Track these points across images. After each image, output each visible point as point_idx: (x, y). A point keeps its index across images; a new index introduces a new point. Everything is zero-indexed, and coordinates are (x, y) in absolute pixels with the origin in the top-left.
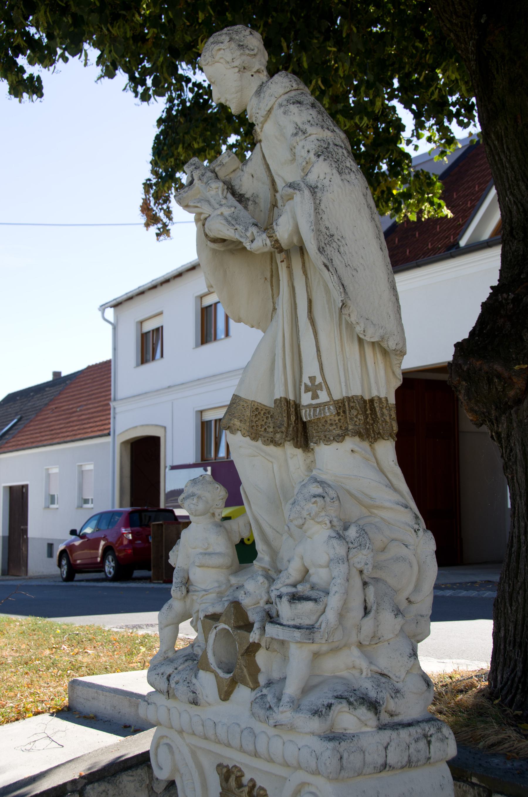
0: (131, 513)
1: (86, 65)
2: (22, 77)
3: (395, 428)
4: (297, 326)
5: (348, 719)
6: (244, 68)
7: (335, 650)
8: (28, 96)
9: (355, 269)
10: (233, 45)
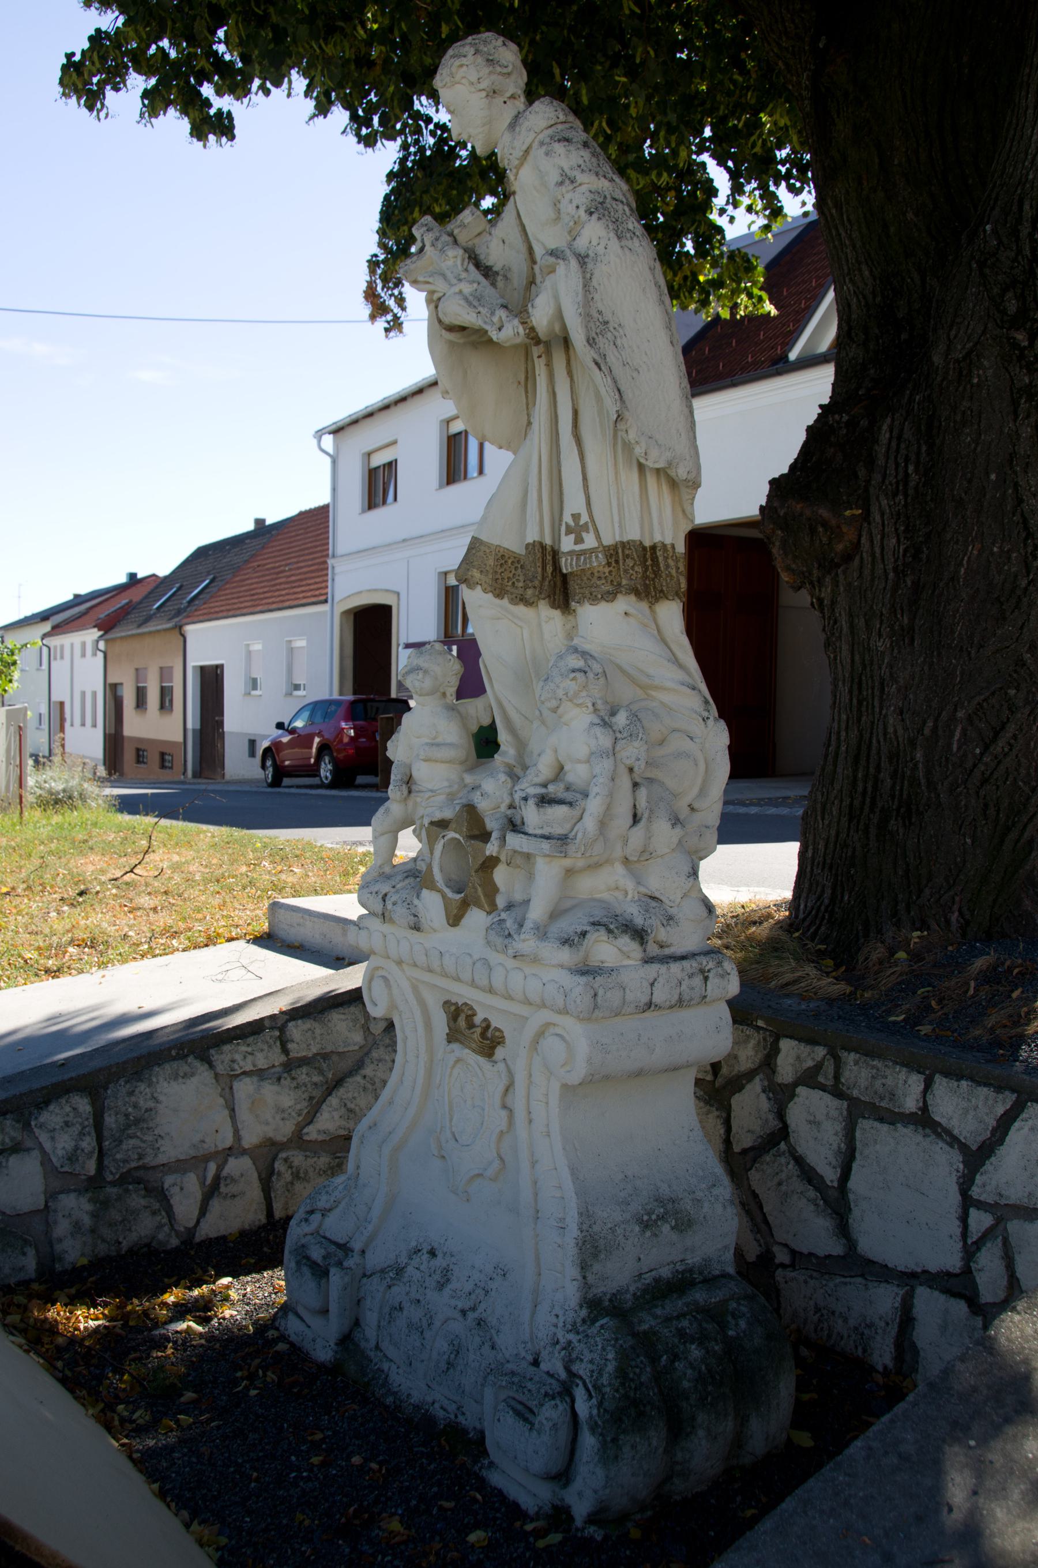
0: (353, 703)
1: (289, 95)
2: (208, 113)
3: (684, 585)
4: (558, 446)
5: (606, 950)
6: (494, 92)
7: (595, 866)
8: (215, 138)
9: (636, 370)
10: (480, 59)
